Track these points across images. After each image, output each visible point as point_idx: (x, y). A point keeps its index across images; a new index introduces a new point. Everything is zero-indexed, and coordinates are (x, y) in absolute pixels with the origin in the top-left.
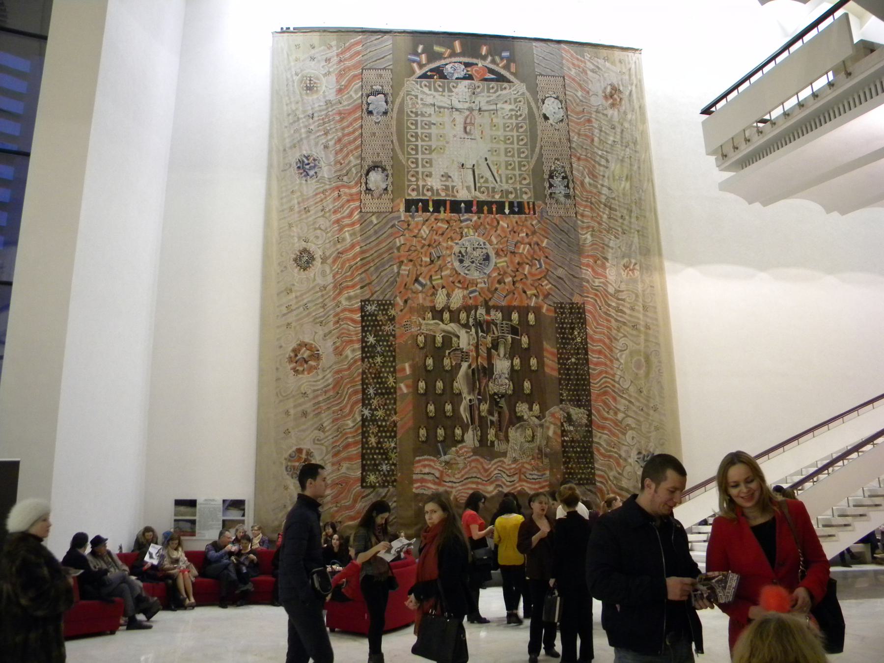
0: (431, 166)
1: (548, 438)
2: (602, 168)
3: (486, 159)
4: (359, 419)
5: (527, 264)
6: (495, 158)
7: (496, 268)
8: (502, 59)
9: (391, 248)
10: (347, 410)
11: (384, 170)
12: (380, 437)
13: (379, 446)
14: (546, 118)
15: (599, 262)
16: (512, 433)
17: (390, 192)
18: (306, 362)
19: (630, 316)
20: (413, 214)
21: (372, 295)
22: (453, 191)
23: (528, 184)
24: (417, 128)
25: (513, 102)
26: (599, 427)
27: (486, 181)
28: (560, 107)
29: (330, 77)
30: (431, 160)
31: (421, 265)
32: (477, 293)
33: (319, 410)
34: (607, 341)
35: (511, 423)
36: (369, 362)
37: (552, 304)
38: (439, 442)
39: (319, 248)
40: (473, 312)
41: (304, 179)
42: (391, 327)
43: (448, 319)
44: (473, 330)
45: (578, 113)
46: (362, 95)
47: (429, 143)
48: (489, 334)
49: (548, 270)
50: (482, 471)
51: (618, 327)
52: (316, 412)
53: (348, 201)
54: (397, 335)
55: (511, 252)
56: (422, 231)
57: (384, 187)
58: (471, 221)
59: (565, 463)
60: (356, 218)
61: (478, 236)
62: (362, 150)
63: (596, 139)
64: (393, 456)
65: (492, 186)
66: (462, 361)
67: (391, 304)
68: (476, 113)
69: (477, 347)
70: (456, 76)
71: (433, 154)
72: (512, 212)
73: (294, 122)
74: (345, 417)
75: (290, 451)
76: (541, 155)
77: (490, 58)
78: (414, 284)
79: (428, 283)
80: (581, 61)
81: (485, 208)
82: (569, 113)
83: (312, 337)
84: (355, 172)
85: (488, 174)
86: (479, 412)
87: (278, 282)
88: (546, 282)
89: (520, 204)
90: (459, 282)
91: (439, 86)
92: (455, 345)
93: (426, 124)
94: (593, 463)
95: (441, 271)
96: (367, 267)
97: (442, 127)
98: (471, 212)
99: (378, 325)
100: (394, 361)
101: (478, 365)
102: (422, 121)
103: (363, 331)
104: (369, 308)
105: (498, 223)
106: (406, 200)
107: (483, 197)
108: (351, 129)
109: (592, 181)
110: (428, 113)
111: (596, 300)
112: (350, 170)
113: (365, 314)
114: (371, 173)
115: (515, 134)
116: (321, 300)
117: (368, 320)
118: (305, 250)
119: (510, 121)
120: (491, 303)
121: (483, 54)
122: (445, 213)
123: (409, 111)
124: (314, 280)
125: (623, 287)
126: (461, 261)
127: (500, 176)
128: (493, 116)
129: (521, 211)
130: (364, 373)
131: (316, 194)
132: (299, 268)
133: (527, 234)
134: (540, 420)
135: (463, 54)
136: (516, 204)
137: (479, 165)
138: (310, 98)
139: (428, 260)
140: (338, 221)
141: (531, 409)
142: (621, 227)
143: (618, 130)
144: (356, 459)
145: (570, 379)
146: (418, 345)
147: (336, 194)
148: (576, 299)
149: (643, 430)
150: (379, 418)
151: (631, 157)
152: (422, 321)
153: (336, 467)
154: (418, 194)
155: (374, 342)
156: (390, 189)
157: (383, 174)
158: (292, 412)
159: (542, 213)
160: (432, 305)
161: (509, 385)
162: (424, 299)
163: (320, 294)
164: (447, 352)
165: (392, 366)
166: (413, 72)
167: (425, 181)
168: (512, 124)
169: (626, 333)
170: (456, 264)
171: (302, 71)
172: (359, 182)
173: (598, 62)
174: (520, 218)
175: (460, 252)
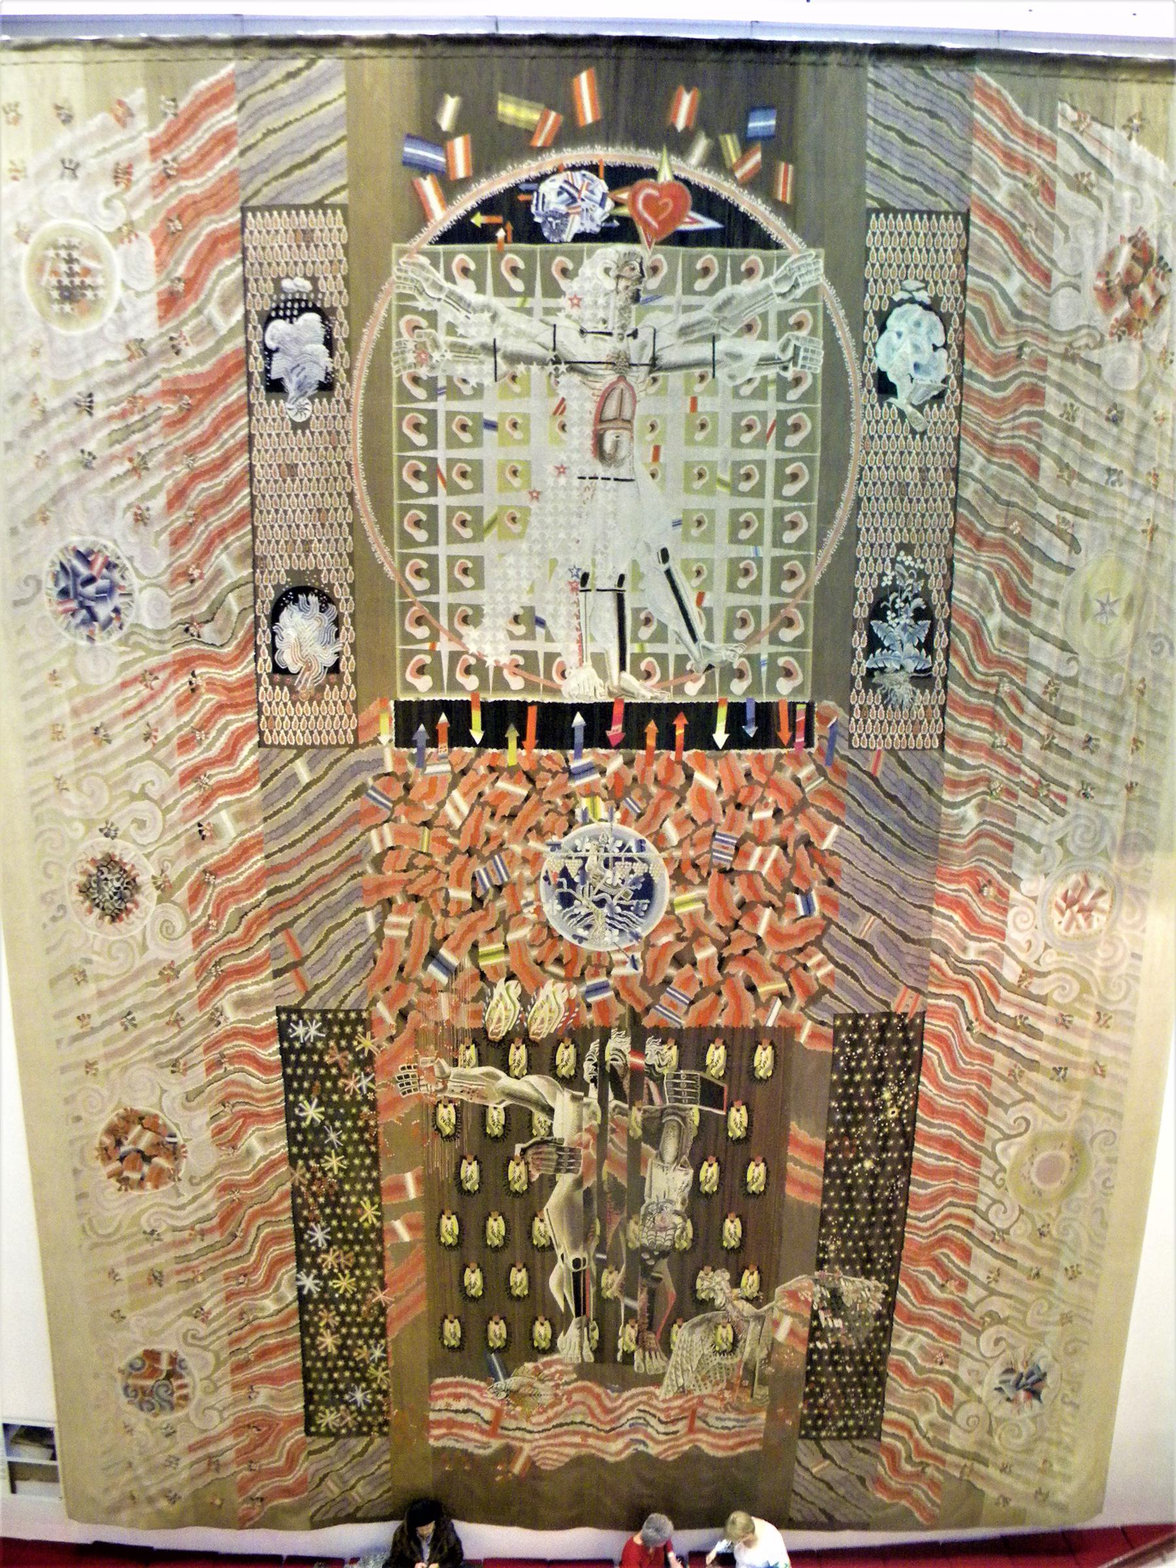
0: (479, 585)
1: (774, 1345)
2: (1051, 575)
3: (665, 555)
4: (291, 1295)
5: (769, 904)
6: (693, 551)
7: (671, 919)
8: (746, 144)
9: (355, 860)
10: (260, 1277)
11: (327, 600)
12: (345, 1337)
13: (363, 1284)
14: (885, 387)
15: (989, 892)
16: (680, 1334)
17: (347, 679)
18: (147, 1159)
19: (1056, 1042)
20: (421, 752)
21: (308, 995)
22: (548, 675)
23: (799, 641)
24: (433, 444)
25: (773, 328)
26: (910, 1318)
27: (661, 635)
28: (940, 341)
29: (134, 247)
30: (478, 561)
31: (445, 913)
32: (610, 994)
33: (190, 1275)
34: (972, 1112)
35: (680, 1314)
36: (309, 1168)
37: (828, 1019)
38: (492, 1350)
39: (148, 856)
40: (594, 1046)
41: (84, 631)
42: (365, 1082)
43: (524, 1062)
44: (593, 1092)
45: (997, 366)
46: (247, 314)
47: (473, 500)
48: (638, 1104)
49: (830, 921)
50: (598, 1411)
51: (1011, 1072)
52: (183, 1277)
53: (220, 708)
54: (381, 1102)
55: (723, 871)
56: (448, 808)
57: (330, 661)
58: (603, 772)
59: (806, 1396)
60: (248, 764)
61: (623, 821)
62: (254, 529)
63: (1047, 464)
64: (380, 1374)
65: (681, 650)
66: (558, 1170)
67: (360, 1020)
68: (638, 377)
69: (600, 1137)
70: (575, 225)
71: (488, 538)
72: (737, 740)
73: (36, 425)
74: (255, 1291)
75: (130, 1357)
76: (853, 533)
77: (701, 146)
78: (425, 967)
79: (468, 963)
80: (1040, 141)
81: (652, 728)
82: (968, 365)
83: (155, 1100)
84: (236, 609)
85: (668, 611)
86: (599, 1290)
87: (49, 951)
88: (820, 956)
89: (765, 712)
90: (558, 961)
91: (514, 270)
92: (540, 1132)
93: (464, 427)
94: (881, 1397)
95: (506, 930)
96: (287, 917)
97: (517, 435)
98: (605, 743)
99: (328, 1076)
100: (376, 1164)
101: (600, 1182)
102: (451, 415)
103: (288, 1088)
104: (300, 1030)
105: (689, 777)
106: (397, 704)
107: (645, 692)
108: (212, 453)
109: (1010, 623)
110: (473, 382)
111: (961, 1002)
112: (220, 603)
113: (291, 1047)
114: (285, 615)
115: (770, 453)
116: (169, 1004)
117: (298, 1063)
118: (110, 862)
119: (760, 405)
120: (647, 1022)
121: (681, 125)
122: (520, 746)
123: (405, 375)
124: (144, 948)
125: (1050, 961)
126: (566, 900)
127: (708, 613)
128: (698, 388)
129: (766, 739)
130: (295, 1192)
131: (125, 685)
132: (97, 911)
133: (777, 813)
134: (759, 1306)
135: (603, 132)
136: (750, 714)
137: (639, 576)
138: (77, 332)
139: (466, 895)
140: (192, 775)
141: (736, 1283)
142: (1078, 775)
143: (1131, 426)
144: (290, 1377)
145: (852, 1211)
146: (439, 1130)
147: (181, 685)
148: (904, 1003)
149: (1029, 1321)
150: (343, 1296)
151: (1155, 529)
152: (448, 1069)
153: (243, 1392)
154: (437, 686)
155: (319, 1118)
156: (347, 668)
157: (325, 616)
158: (123, 1272)
159: (832, 741)
160: (479, 1024)
161: (684, 1229)
162: (455, 1009)
163: (163, 988)
164: (518, 1148)
165: (369, 1179)
166: (423, 216)
167: (459, 637)
168: (763, 415)
169: (1031, 1090)
170: (552, 908)
171: (40, 219)
172: (250, 642)
173: (1101, 143)
174: (760, 759)
175: (565, 873)
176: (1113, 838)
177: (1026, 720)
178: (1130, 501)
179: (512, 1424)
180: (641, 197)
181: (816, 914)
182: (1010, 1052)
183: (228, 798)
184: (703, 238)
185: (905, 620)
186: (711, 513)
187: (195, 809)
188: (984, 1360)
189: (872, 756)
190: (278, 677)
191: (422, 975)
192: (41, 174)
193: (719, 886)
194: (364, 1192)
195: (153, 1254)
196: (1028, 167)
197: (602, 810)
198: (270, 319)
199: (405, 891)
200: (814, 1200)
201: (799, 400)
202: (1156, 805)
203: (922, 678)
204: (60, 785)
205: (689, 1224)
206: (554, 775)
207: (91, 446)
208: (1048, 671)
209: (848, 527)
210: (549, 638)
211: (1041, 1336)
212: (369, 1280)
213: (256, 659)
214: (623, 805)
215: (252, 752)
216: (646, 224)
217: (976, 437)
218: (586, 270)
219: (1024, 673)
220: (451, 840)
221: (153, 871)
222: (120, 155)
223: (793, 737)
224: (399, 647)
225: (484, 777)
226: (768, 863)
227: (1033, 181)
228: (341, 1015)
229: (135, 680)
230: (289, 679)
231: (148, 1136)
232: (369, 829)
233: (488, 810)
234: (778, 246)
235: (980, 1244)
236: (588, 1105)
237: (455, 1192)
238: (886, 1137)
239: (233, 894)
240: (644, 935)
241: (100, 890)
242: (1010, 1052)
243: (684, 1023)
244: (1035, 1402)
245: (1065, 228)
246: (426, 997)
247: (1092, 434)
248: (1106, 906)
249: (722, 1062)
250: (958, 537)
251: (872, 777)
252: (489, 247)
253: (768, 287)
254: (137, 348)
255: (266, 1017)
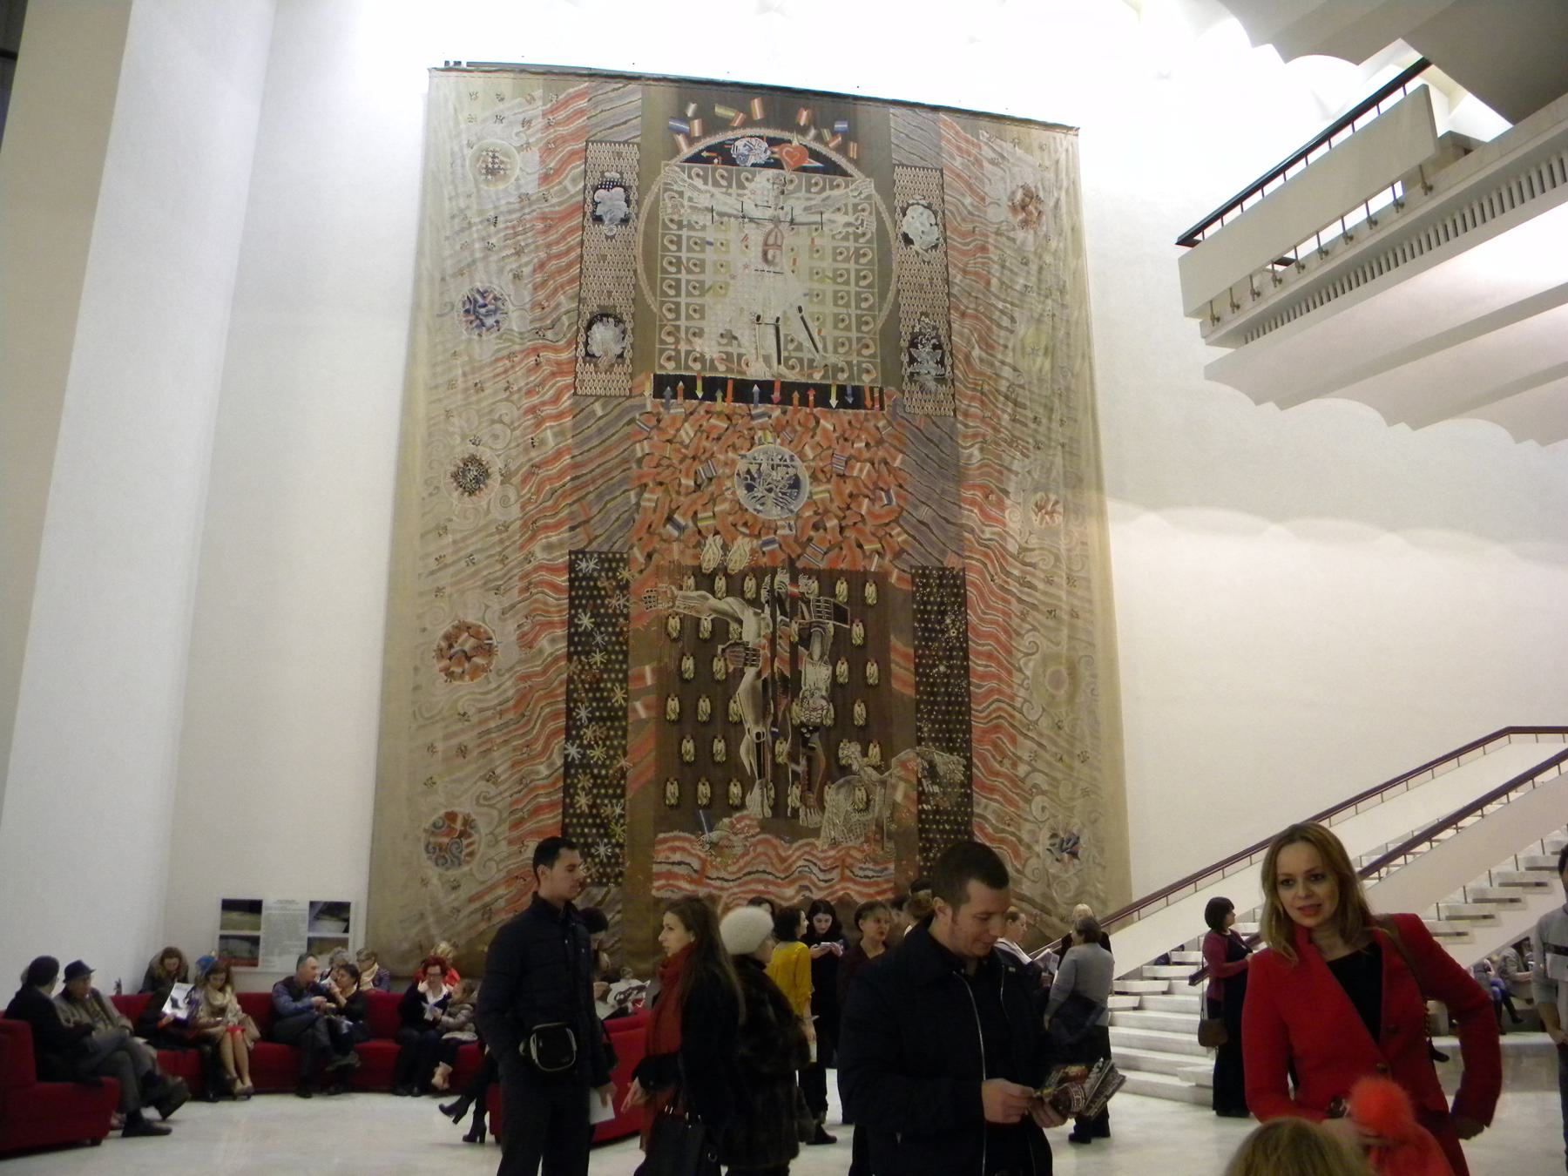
0: (703, 317)
1: (894, 805)
2: (1003, 333)
3: (800, 309)
4: (559, 762)
5: (867, 496)
6: (815, 309)
7: (811, 502)
8: (834, 134)
9: (626, 461)
10: (538, 747)
12: (596, 797)
13: (594, 811)
14: (908, 241)
16: (830, 794)
17: (628, 361)
18: (468, 658)
19: (1045, 593)
20: (668, 401)
21: (590, 542)
22: (739, 363)
23: (873, 356)
24: (679, 249)
27: (799, 348)
30: (702, 307)
31: (678, 493)
32: (776, 546)
33: (489, 746)
35: (830, 778)
38: (700, 807)
40: (768, 579)
41: (477, 332)
43: (724, 589)
44: (767, 610)
45: (963, 235)
46: (585, 186)
48: (795, 619)
49: (902, 509)
50: (775, 860)
51: (1022, 613)
52: (484, 748)
53: (553, 374)
55: (839, 475)
56: (682, 432)
57: (619, 352)
58: (770, 417)
61: (782, 445)
62: (581, 284)
63: (994, 281)
64: (618, 830)
65: (810, 356)
66: (745, 664)
67: (622, 559)
68: (784, 227)
69: (773, 641)
70: (752, 160)
72: (843, 404)
75: (434, 818)
76: (897, 306)
77: (813, 132)
78: (664, 526)
79: (691, 524)
81: (796, 395)
82: (948, 233)
83: (480, 615)
85: (802, 336)
86: (774, 756)
87: (424, 515)
88: (899, 529)
89: (857, 391)
90: (745, 524)
91: (722, 177)
92: (734, 636)
93: (696, 243)
96: (583, 492)
97: (723, 249)
98: (771, 402)
99: (599, 596)
100: (625, 661)
102: (689, 238)
104: (583, 565)
105: (818, 422)
106: (655, 376)
107: (792, 376)
108: (562, 247)
109: (984, 355)
110: (701, 224)
114: (595, 327)
115: (852, 266)
116: (498, 549)
117: (580, 587)
118: (474, 459)
119: (846, 244)
120: (799, 565)
121: (802, 123)
122: (723, 400)
124: (488, 511)
125: (1034, 542)
126: (750, 488)
127: (824, 339)
128: (815, 234)
130: (570, 680)
131: (497, 360)
132: (461, 489)
133: (867, 445)
134: (882, 773)
135: (765, 123)
136: (849, 391)
137: (787, 319)
138: (492, 188)
139: (692, 483)
140: (533, 410)
141: (865, 754)
143: (1034, 268)
146: (669, 635)
147: (532, 360)
148: (951, 561)
150: (596, 763)
151: (1054, 315)
152: (676, 592)
153: (515, 848)
154: (678, 367)
155: (590, 626)
158: (440, 746)
160: (695, 563)
161: (828, 710)
162: (682, 552)
163: (497, 537)
164: (720, 647)
165: (621, 670)
168: (848, 249)
169: (1036, 624)
170: (741, 493)
174: (856, 415)
175: (749, 472)
176: (1058, 472)
177: (1000, 406)
178: (1039, 302)
179: (714, 874)
180: (785, 151)
181: (894, 503)
182: (1020, 600)
183: (553, 424)
184: (815, 170)
185: (928, 349)
186: (824, 292)
187: (529, 430)
188: (1036, 821)
189: (917, 418)
190: (588, 358)
191: (662, 531)
192: (484, 121)
193: (838, 485)
194: (617, 679)
195: (463, 731)
196: (969, 154)
197: (770, 438)
198: (597, 189)
199: (655, 480)
200: (910, 692)
201: (866, 243)
202: (1079, 456)
203: (940, 379)
204: (448, 414)
205: (831, 707)
206: (743, 417)
207: (493, 241)
208: (1008, 380)
209: (894, 303)
210: (739, 346)
211: (1071, 809)
212: (615, 748)
213: (576, 349)
214: (781, 435)
215: (569, 398)
216: (787, 163)
217: (956, 266)
218: (757, 179)
219: (996, 381)
220: (683, 450)
221: (501, 465)
222: (528, 115)
223: (873, 405)
224: (657, 346)
225: (703, 417)
226: (865, 472)
227: (972, 159)
228: (610, 556)
229: (503, 358)
230: (594, 360)
231: (472, 642)
232: (636, 442)
233: (705, 435)
234: (851, 176)
235: (1021, 733)
236: (764, 619)
237: (677, 678)
238: (951, 650)
239: (550, 479)
240: (796, 510)
241: (464, 476)
242: (1020, 600)
243: (822, 565)
244: (1076, 861)
245: (990, 180)
246: (665, 545)
247: (1015, 270)
248: (1061, 510)
249: (845, 593)
250: (952, 311)
251: (917, 428)
252: (710, 166)
253: (847, 193)
254: (525, 198)
255: (562, 556)
